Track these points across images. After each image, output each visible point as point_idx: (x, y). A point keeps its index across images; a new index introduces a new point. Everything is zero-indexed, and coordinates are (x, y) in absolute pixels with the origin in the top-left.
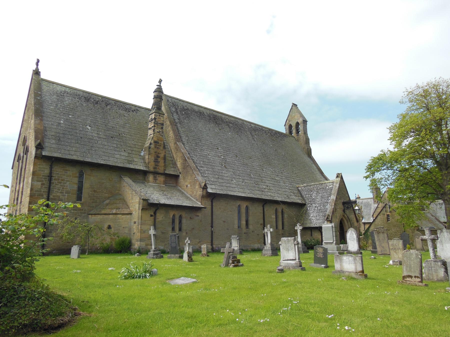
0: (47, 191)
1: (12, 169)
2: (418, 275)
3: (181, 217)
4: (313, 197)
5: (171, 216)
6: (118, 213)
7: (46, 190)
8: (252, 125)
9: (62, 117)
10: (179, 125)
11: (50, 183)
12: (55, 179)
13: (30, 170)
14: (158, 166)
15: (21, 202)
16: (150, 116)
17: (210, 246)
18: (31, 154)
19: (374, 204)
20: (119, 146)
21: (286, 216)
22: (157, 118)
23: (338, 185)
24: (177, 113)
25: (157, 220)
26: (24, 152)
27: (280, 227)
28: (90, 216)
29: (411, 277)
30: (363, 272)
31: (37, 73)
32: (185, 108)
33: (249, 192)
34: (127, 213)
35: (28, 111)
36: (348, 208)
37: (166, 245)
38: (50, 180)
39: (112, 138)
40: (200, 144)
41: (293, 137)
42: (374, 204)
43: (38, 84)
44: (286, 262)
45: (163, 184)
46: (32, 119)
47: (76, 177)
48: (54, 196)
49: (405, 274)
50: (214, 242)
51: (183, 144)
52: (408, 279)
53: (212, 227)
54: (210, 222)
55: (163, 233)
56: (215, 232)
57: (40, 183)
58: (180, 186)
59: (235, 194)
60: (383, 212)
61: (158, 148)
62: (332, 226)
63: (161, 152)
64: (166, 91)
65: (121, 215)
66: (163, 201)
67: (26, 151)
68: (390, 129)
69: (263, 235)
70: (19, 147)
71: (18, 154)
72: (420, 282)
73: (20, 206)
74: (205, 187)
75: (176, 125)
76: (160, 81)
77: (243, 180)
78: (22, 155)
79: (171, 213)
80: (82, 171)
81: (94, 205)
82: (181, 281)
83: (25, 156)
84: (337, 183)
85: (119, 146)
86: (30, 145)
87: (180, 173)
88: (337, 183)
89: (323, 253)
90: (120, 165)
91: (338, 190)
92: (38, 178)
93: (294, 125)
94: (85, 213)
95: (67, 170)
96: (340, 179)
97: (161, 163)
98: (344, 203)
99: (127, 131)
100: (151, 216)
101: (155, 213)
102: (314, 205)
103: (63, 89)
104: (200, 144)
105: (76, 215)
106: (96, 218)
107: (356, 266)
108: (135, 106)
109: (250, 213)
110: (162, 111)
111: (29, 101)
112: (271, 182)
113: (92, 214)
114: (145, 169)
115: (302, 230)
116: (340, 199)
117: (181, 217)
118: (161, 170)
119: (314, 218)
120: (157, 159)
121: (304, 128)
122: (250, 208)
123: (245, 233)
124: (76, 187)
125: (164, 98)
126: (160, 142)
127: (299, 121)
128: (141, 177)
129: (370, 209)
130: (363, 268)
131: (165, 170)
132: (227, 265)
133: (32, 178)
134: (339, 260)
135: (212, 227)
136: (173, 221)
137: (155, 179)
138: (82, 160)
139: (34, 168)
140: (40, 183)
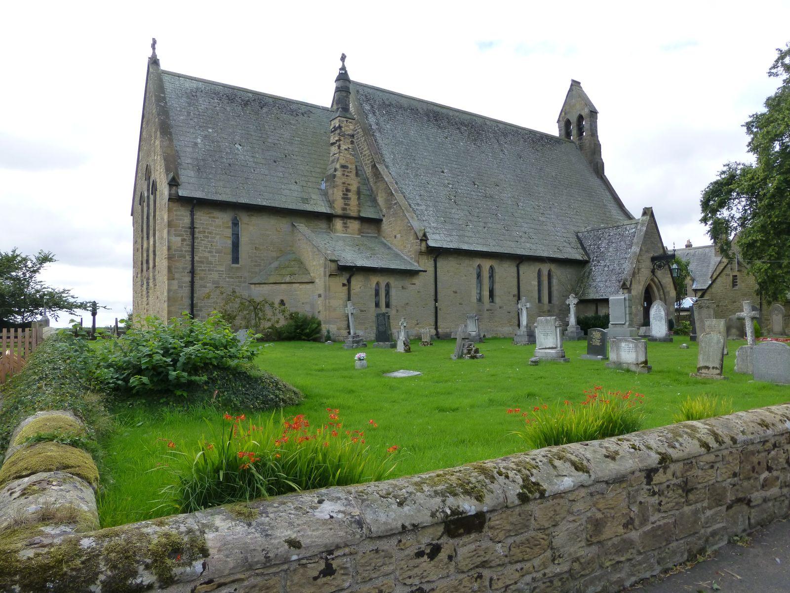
0: (190, 250)
1: (132, 215)
2: (718, 366)
3: (388, 285)
4: (602, 249)
5: (374, 285)
6: (294, 281)
7: (189, 248)
8: (501, 126)
9: (199, 132)
10: (377, 134)
11: (193, 238)
12: (199, 232)
13: (162, 219)
14: (348, 205)
15: (154, 266)
16: (332, 123)
17: (433, 332)
18: (162, 194)
19: (716, 255)
20: (287, 175)
21: (555, 281)
22: (343, 125)
23: (645, 229)
24: (374, 113)
25: (352, 292)
26: (148, 190)
27: (545, 299)
28: (252, 286)
29: (707, 368)
30: (646, 362)
31: (154, 62)
32: (387, 102)
33: (494, 243)
34: (306, 280)
35: (147, 124)
36: (660, 266)
37: (367, 328)
38: (193, 234)
39: (275, 162)
40: (414, 165)
41: (572, 142)
42: (716, 255)
43: (158, 81)
44: (543, 351)
45: (359, 234)
46: (155, 138)
47: (228, 227)
48: (200, 257)
49: (701, 364)
50: (439, 324)
51: (387, 167)
52: (703, 371)
53: (436, 300)
54: (433, 293)
55: (362, 311)
56: (440, 310)
57: (179, 239)
58: (384, 237)
59: (472, 248)
60: (728, 271)
61: (347, 176)
62: (625, 299)
63: (352, 182)
64: (354, 76)
65: (298, 285)
66: (360, 263)
67: (153, 188)
68: (749, 126)
69: (517, 313)
70: (139, 182)
71: (138, 194)
72: (718, 374)
73: (154, 272)
74: (424, 238)
75: (373, 135)
76: (343, 58)
77: (485, 223)
78: (146, 195)
79: (374, 280)
80: (236, 218)
81: (257, 269)
82: (401, 374)
83: (152, 197)
84: (643, 225)
85: (287, 175)
86: (158, 180)
87: (384, 216)
88: (643, 225)
89: (601, 339)
90: (290, 207)
91: (645, 237)
92: (175, 231)
93: (574, 119)
94: (245, 282)
95: (214, 218)
96: (648, 217)
97: (354, 201)
98: (653, 259)
99: (297, 149)
100: (344, 285)
101: (349, 281)
102: (602, 263)
103: (194, 85)
104: (414, 165)
105: (233, 285)
106: (261, 289)
107: (637, 356)
108: (306, 105)
109: (497, 278)
110: (351, 114)
111: (147, 109)
112: (532, 226)
113: (255, 284)
114: (328, 211)
115: (577, 305)
116: (647, 252)
117: (388, 285)
118: (353, 211)
119: (602, 284)
120: (347, 195)
121: (591, 125)
122: (496, 267)
123: (487, 310)
124: (229, 242)
125: (352, 88)
126: (350, 166)
127: (583, 114)
128: (323, 225)
129: (708, 266)
130: (646, 356)
131: (359, 211)
132: (461, 357)
133: (169, 232)
134: (615, 348)
135: (436, 300)
136: (377, 294)
137: (346, 227)
138: (234, 200)
139: (169, 216)
140: (179, 239)
